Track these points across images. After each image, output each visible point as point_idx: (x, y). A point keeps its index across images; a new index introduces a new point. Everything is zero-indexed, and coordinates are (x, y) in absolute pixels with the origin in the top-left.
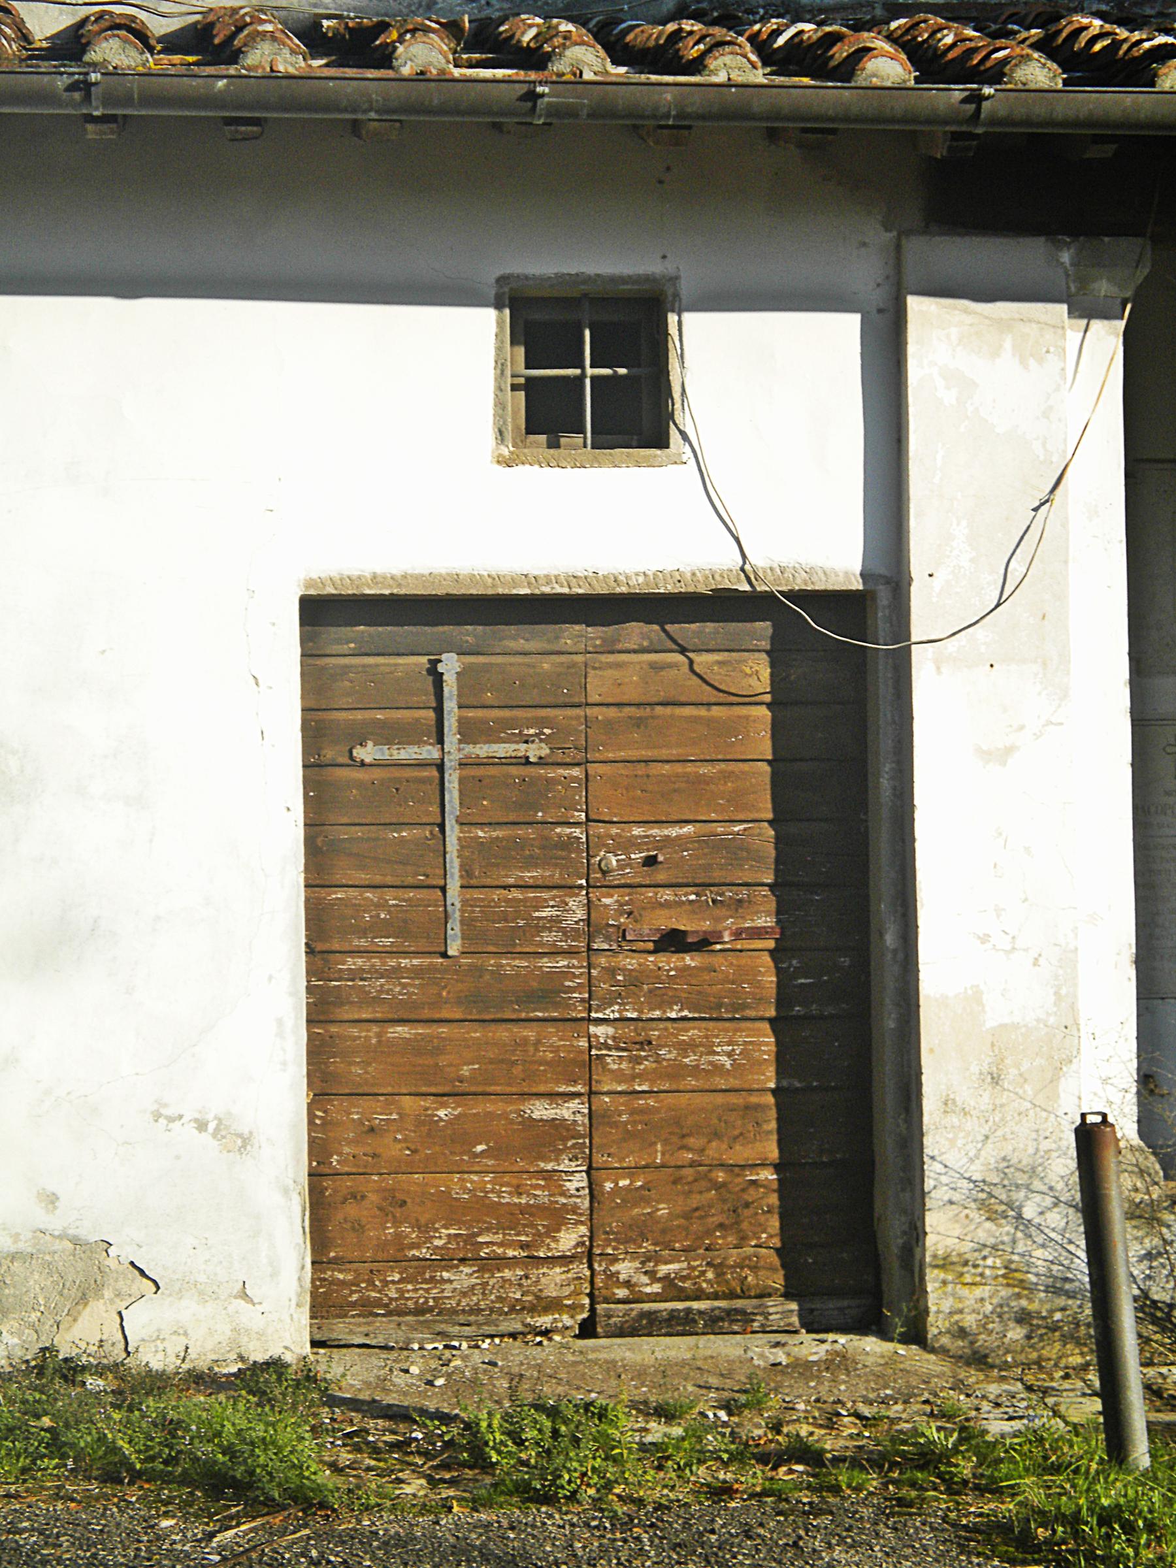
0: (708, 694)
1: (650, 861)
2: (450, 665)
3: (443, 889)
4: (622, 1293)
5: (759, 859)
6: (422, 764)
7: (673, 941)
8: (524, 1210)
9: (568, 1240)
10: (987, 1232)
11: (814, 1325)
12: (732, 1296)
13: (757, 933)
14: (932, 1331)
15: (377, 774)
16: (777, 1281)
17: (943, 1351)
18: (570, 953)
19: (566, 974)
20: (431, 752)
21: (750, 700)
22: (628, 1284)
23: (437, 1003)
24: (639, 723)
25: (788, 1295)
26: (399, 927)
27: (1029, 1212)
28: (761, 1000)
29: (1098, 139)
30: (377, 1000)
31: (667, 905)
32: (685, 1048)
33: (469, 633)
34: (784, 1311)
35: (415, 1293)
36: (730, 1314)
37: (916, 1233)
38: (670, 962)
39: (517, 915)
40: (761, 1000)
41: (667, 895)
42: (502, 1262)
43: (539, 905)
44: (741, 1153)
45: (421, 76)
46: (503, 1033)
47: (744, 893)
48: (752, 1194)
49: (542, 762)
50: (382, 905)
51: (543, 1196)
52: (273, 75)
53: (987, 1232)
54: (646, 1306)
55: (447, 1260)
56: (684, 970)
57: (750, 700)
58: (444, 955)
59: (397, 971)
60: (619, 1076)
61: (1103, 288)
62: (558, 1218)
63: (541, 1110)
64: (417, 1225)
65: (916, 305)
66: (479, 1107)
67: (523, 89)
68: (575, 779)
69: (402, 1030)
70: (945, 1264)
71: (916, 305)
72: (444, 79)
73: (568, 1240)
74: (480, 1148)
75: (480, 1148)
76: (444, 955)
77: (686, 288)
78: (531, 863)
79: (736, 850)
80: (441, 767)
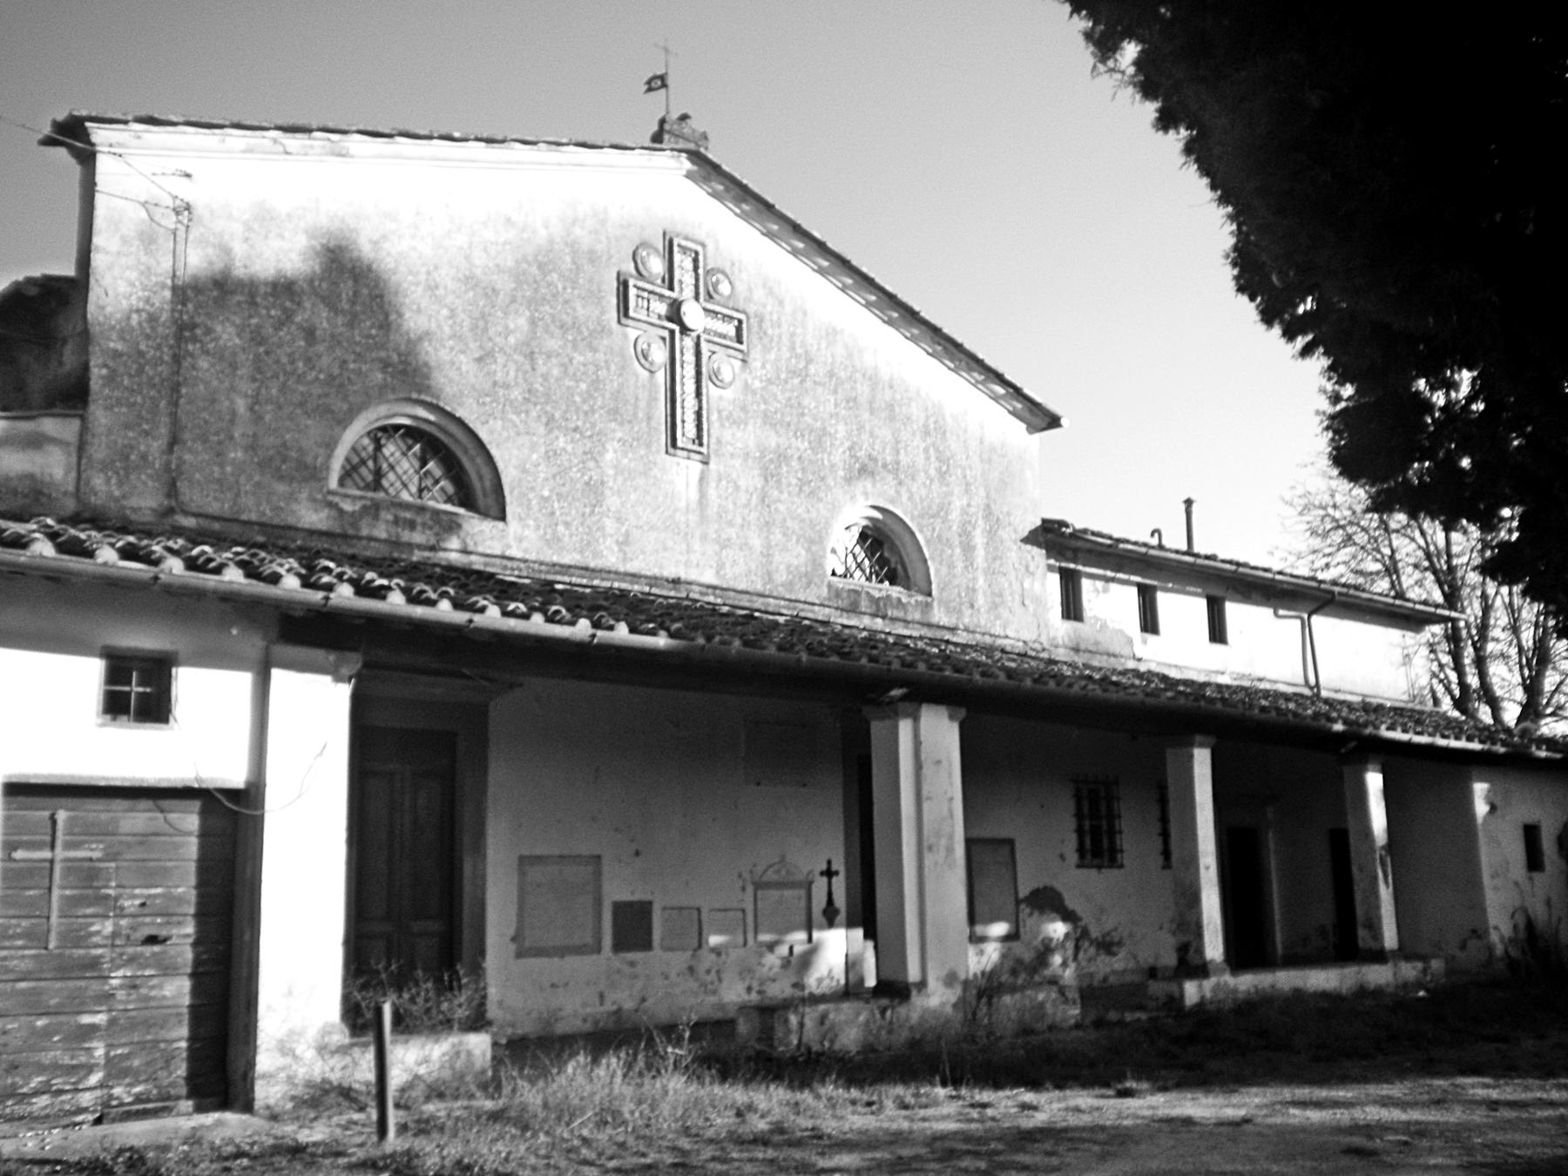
0: (171, 831)
1: (143, 905)
2: (62, 816)
3: (48, 918)
4: (114, 1103)
5: (188, 902)
6: (44, 860)
7: (152, 940)
8: (74, 1067)
9: (94, 1079)
10: (281, 1061)
11: (200, 1109)
12: (163, 1100)
13: (187, 936)
14: (256, 1107)
15: (22, 865)
16: (184, 1091)
17: (261, 1117)
18: (104, 946)
19: (102, 956)
20: (47, 854)
21: (189, 834)
22: (117, 1098)
23: (42, 971)
24: (141, 843)
25: (188, 1097)
26: (28, 935)
27: (298, 1052)
28: (186, 965)
29: (360, 617)
30: (12, 971)
31: (148, 924)
32: (153, 988)
33: (70, 802)
34: (187, 1105)
35: (20, 1110)
36: (164, 1109)
37: (251, 1064)
38: (149, 950)
39: (80, 930)
40: (186, 965)
41: (148, 920)
42: (60, 1092)
43: (92, 924)
44: (174, 1034)
45: (105, 564)
46: (71, 984)
47: (181, 919)
48: (178, 1052)
49: (99, 860)
50: (18, 926)
51: (83, 1059)
52: (41, 556)
53: (281, 1061)
54: (127, 1108)
55: (37, 1093)
56: (154, 954)
57: (189, 834)
58: (46, 948)
59: (23, 957)
60: (121, 1002)
61: (345, 671)
62: (90, 1069)
63: (86, 1019)
64: (23, 1077)
65: (276, 673)
66: (62, 1018)
67: (151, 575)
68: (44, 868)
69: (23, 985)
70: (264, 1076)
71: (276, 673)
72: (113, 566)
73: (94, 1079)
74: (56, 1039)
75: (56, 1039)
76: (46, 948)
77: (182, 656)
78: (89, 905)
79: (180, 900)
80: (52, 861)
